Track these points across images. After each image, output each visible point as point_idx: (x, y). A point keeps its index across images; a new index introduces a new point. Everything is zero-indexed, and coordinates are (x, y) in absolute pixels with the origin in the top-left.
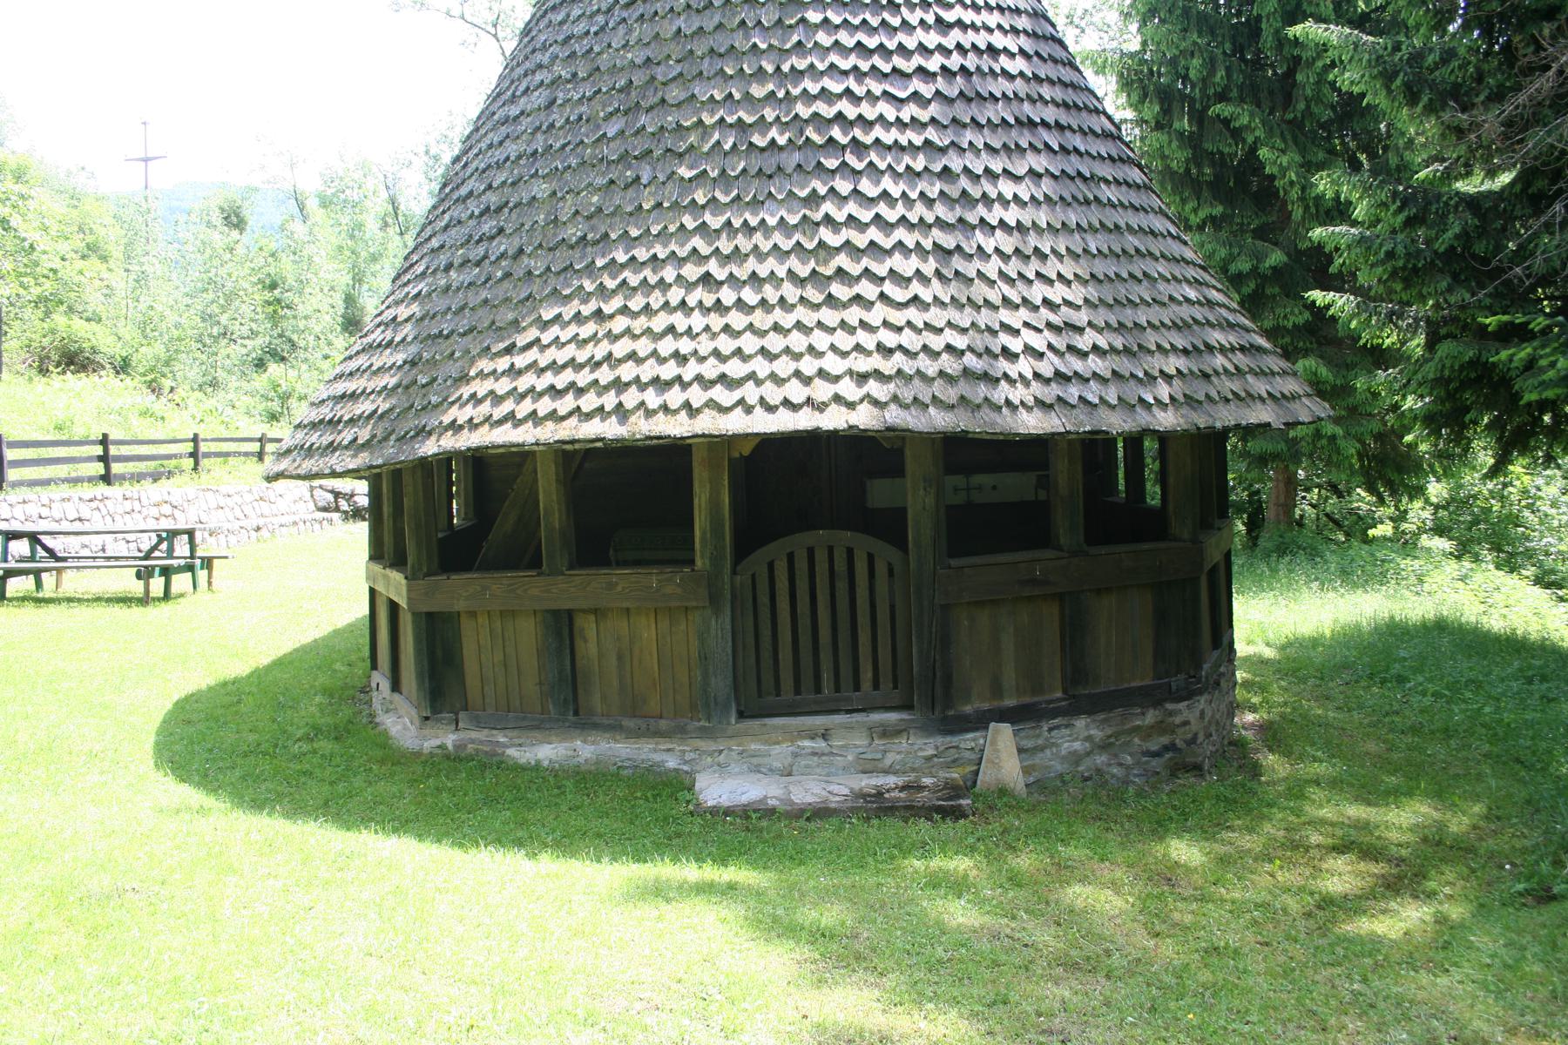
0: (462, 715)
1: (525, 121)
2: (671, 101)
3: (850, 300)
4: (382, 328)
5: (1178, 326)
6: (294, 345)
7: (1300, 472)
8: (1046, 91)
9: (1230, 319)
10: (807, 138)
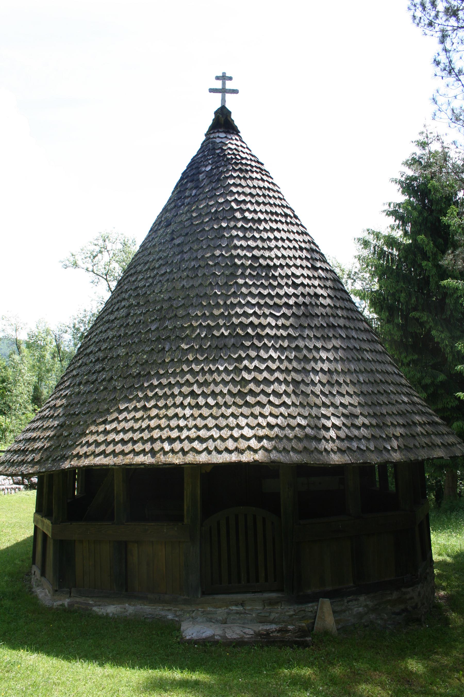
0: (73, 590)
1: (117, 322)
2: (179, 316)
3: (255, 403)
4: (49, 409)
5: (401, 414)
6: (10, 407)
7: (458, 471)
8: (340, 313)
9: (423, 410)
10: (237, 332)
